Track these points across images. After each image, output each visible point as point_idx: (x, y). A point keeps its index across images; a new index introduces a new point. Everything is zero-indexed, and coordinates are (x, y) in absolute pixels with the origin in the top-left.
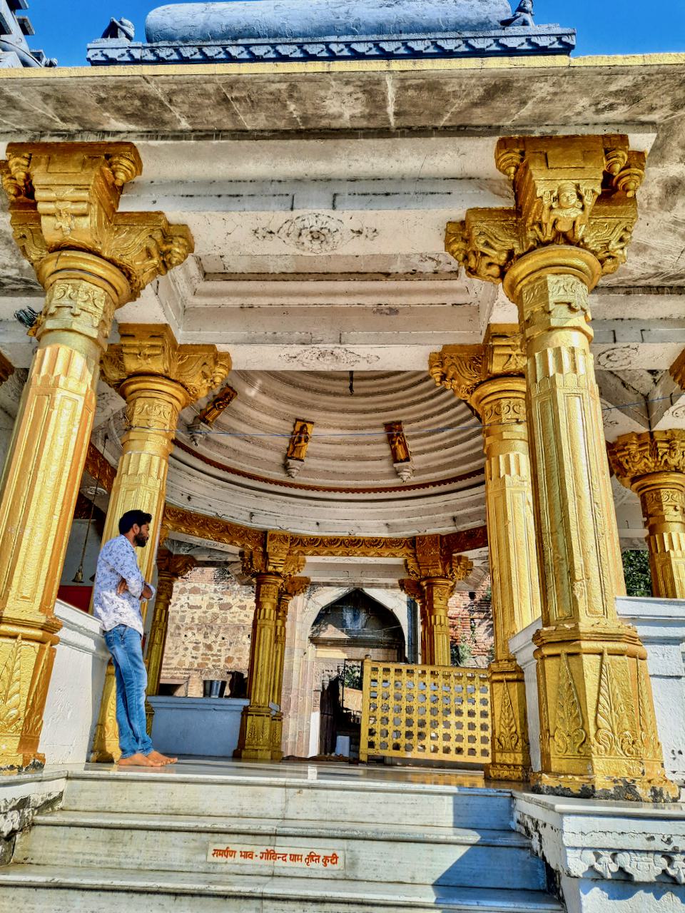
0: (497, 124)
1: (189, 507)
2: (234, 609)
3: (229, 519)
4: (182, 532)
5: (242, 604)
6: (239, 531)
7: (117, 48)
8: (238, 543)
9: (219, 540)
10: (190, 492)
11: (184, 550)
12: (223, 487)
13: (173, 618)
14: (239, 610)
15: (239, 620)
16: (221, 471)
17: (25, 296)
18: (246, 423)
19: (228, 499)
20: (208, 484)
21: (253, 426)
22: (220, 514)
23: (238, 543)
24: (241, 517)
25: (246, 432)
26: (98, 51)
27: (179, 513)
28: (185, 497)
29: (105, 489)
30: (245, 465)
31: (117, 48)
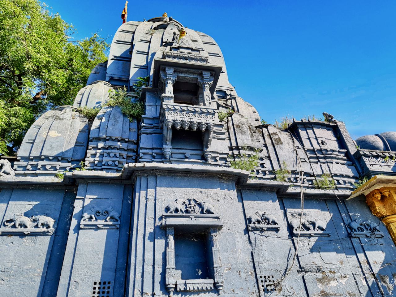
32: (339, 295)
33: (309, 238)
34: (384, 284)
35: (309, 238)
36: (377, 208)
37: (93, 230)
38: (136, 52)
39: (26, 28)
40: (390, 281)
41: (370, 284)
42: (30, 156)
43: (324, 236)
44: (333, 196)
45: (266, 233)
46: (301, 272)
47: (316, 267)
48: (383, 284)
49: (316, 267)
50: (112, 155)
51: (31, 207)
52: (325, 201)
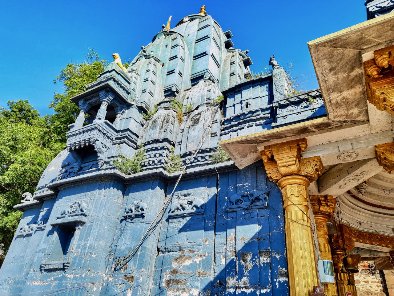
0: (131, 103)
1: (361, 228)
2: (362, 283)
3: (382, 233)
4: (361, 242)
5: (365, 280)
6: (388, 239)
7: (384, 2)
8: (390, 246)
9: (380, 245)
10: (360, 220)
11: (354, 252)
12: (376, 216)
13: (359, 288)
14: (365, 283)
15: (367, 289)
16: (374, 207)
17: (338, 130)
18: (382, 180)
19: (378, 222)
20: (368, 215)
21: (386, 181)
22: (377, 231)
23: (390, 246)
24: (389, 231)
25: (383, 185)
26: (374, 7)
27: (356, 233)
28: (358, 223)
29: (332, 222)
30: (384, 203)
31: (384, 2)
32: (188, 274)
33: (183, 219)
34: (243, 263)
35: (183, 219)
36: (268, 172)
37: (41, 231)
38: (148, 79)
39: (35, 129)
40: (252, 259)
41: (227, 262)
42: (186, 153)
43: (198, 215)
44: (213, 170)
45: (134, 220)
46: (165, 252)
47: (178, 246)
48: (241, 263)
49: (178, 246)
50: (157, 155)
51: (31, 219)
52: (208, 177)
